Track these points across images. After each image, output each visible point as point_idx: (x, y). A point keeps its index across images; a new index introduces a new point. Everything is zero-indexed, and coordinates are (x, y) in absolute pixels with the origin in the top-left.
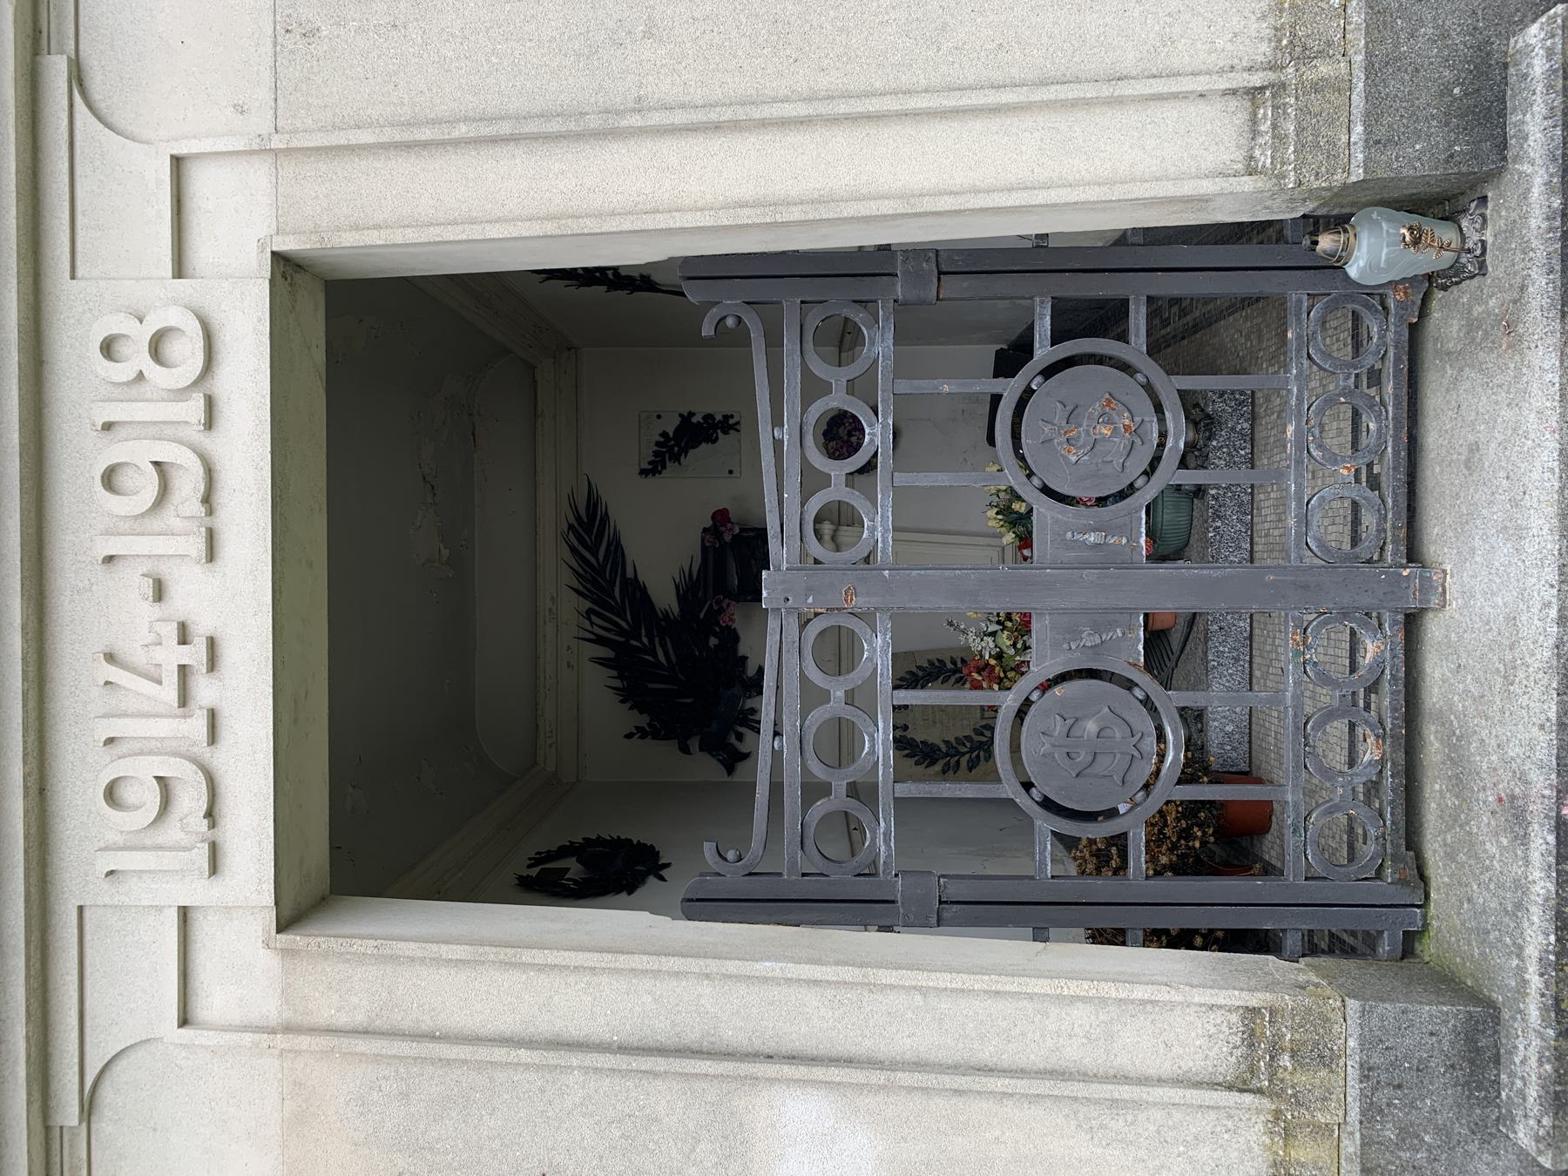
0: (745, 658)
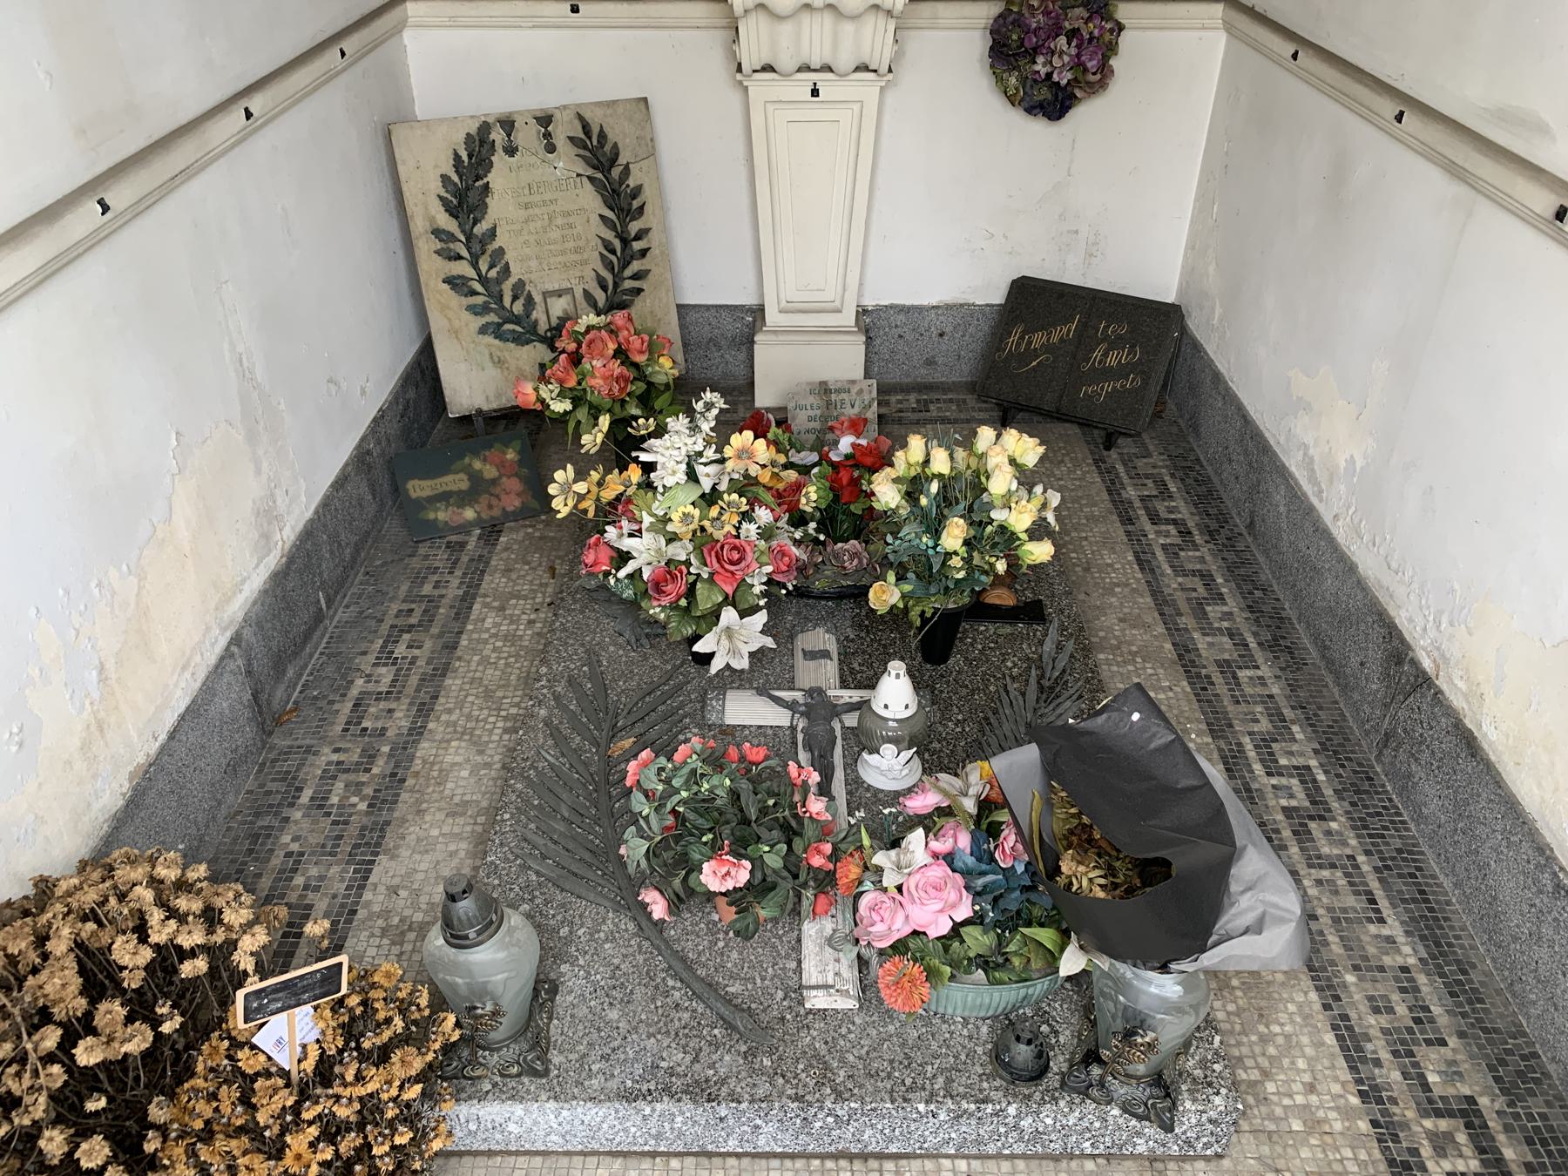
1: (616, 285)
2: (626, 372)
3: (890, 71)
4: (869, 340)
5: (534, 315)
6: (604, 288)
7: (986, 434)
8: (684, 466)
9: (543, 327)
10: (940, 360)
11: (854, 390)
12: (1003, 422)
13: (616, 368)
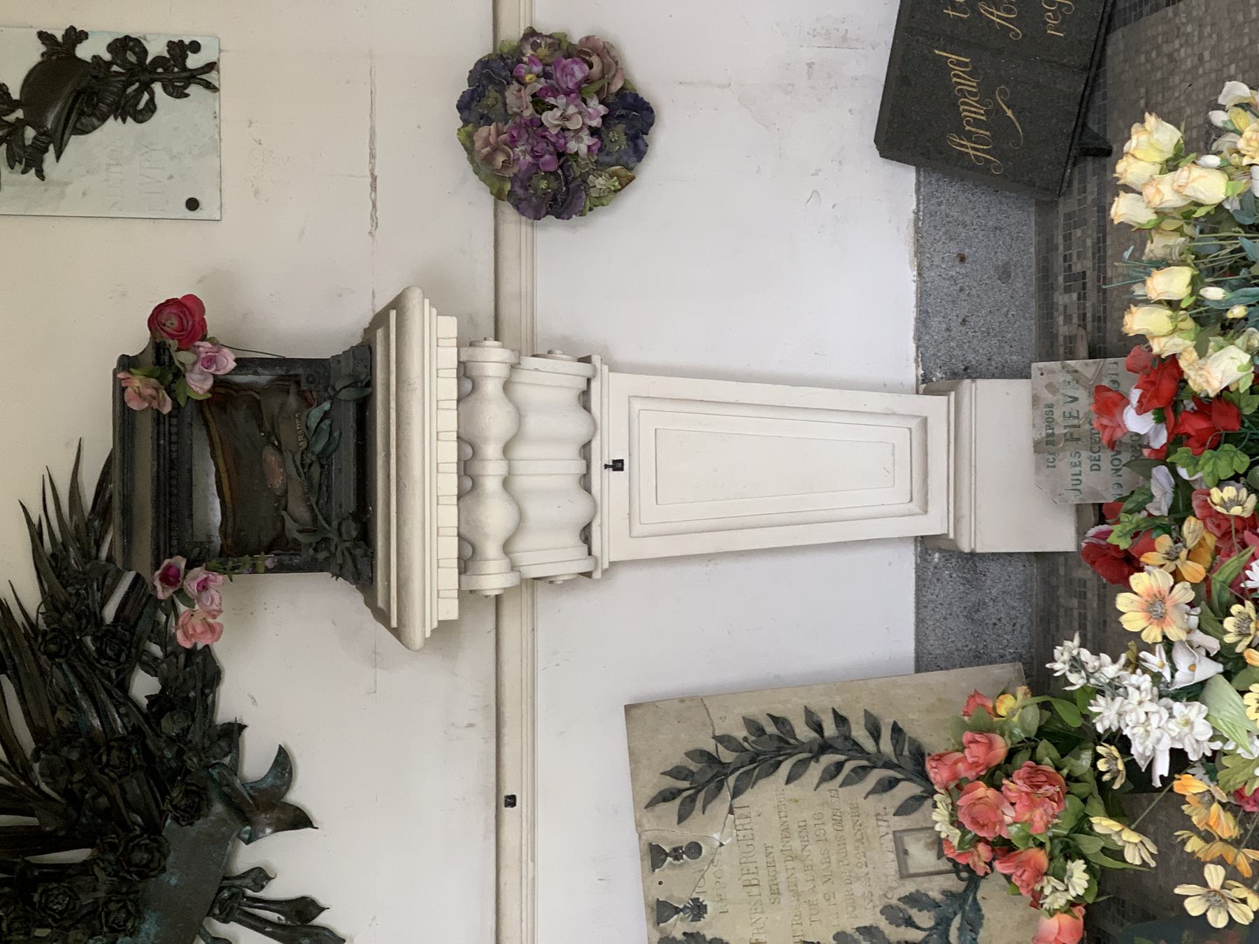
0: (234, 731)
1: (888, 765)
2: (1022, 772)
3: (586, 360)
4: (971, 372)
5: (935, 894)
6: (891, 784)
7: (1123, 209)
8: (1178, 707)
9: (954, 884)
10: (1002, 258)
11: (1048, 397)
12: (1103, 151)
13: (1015, 786)
